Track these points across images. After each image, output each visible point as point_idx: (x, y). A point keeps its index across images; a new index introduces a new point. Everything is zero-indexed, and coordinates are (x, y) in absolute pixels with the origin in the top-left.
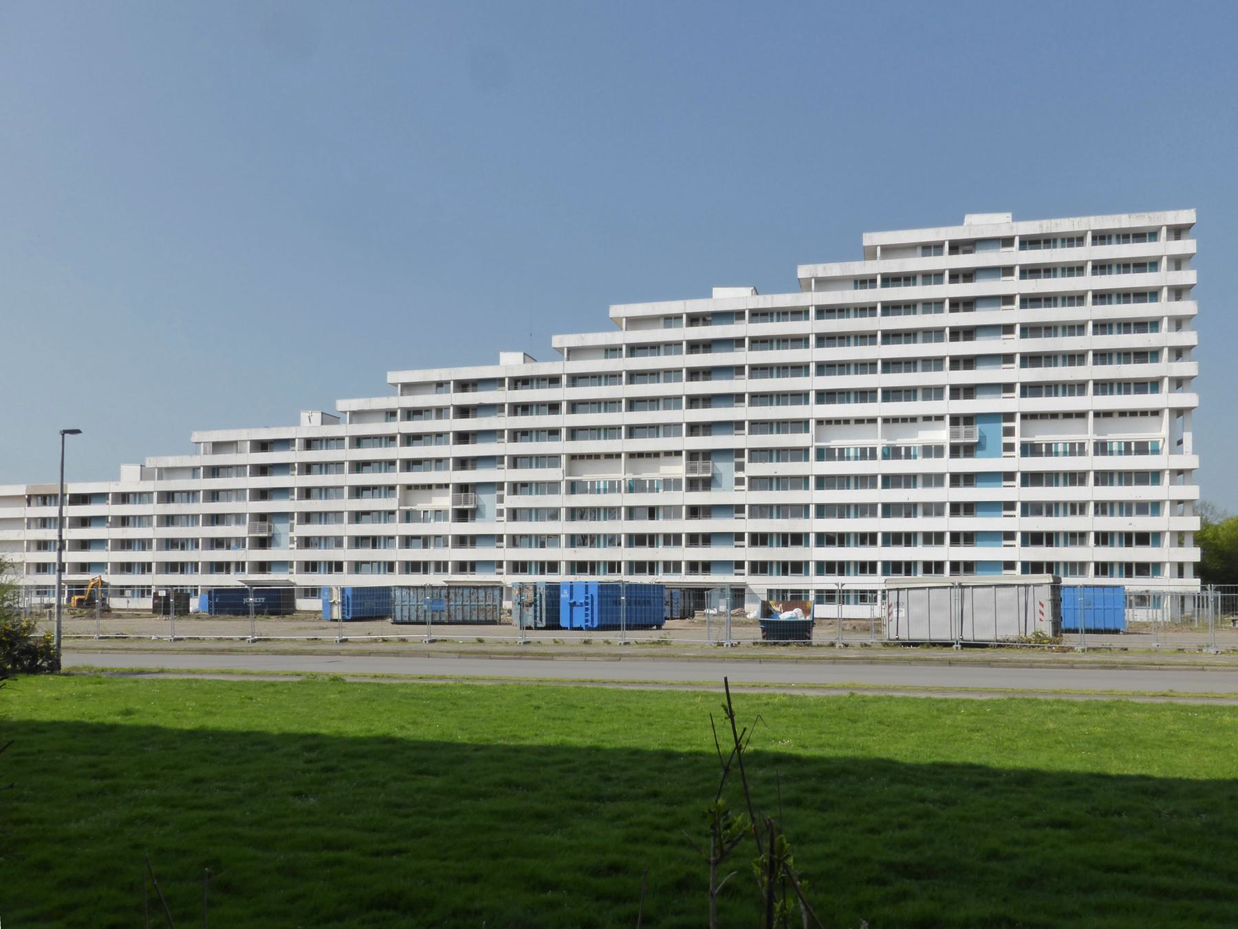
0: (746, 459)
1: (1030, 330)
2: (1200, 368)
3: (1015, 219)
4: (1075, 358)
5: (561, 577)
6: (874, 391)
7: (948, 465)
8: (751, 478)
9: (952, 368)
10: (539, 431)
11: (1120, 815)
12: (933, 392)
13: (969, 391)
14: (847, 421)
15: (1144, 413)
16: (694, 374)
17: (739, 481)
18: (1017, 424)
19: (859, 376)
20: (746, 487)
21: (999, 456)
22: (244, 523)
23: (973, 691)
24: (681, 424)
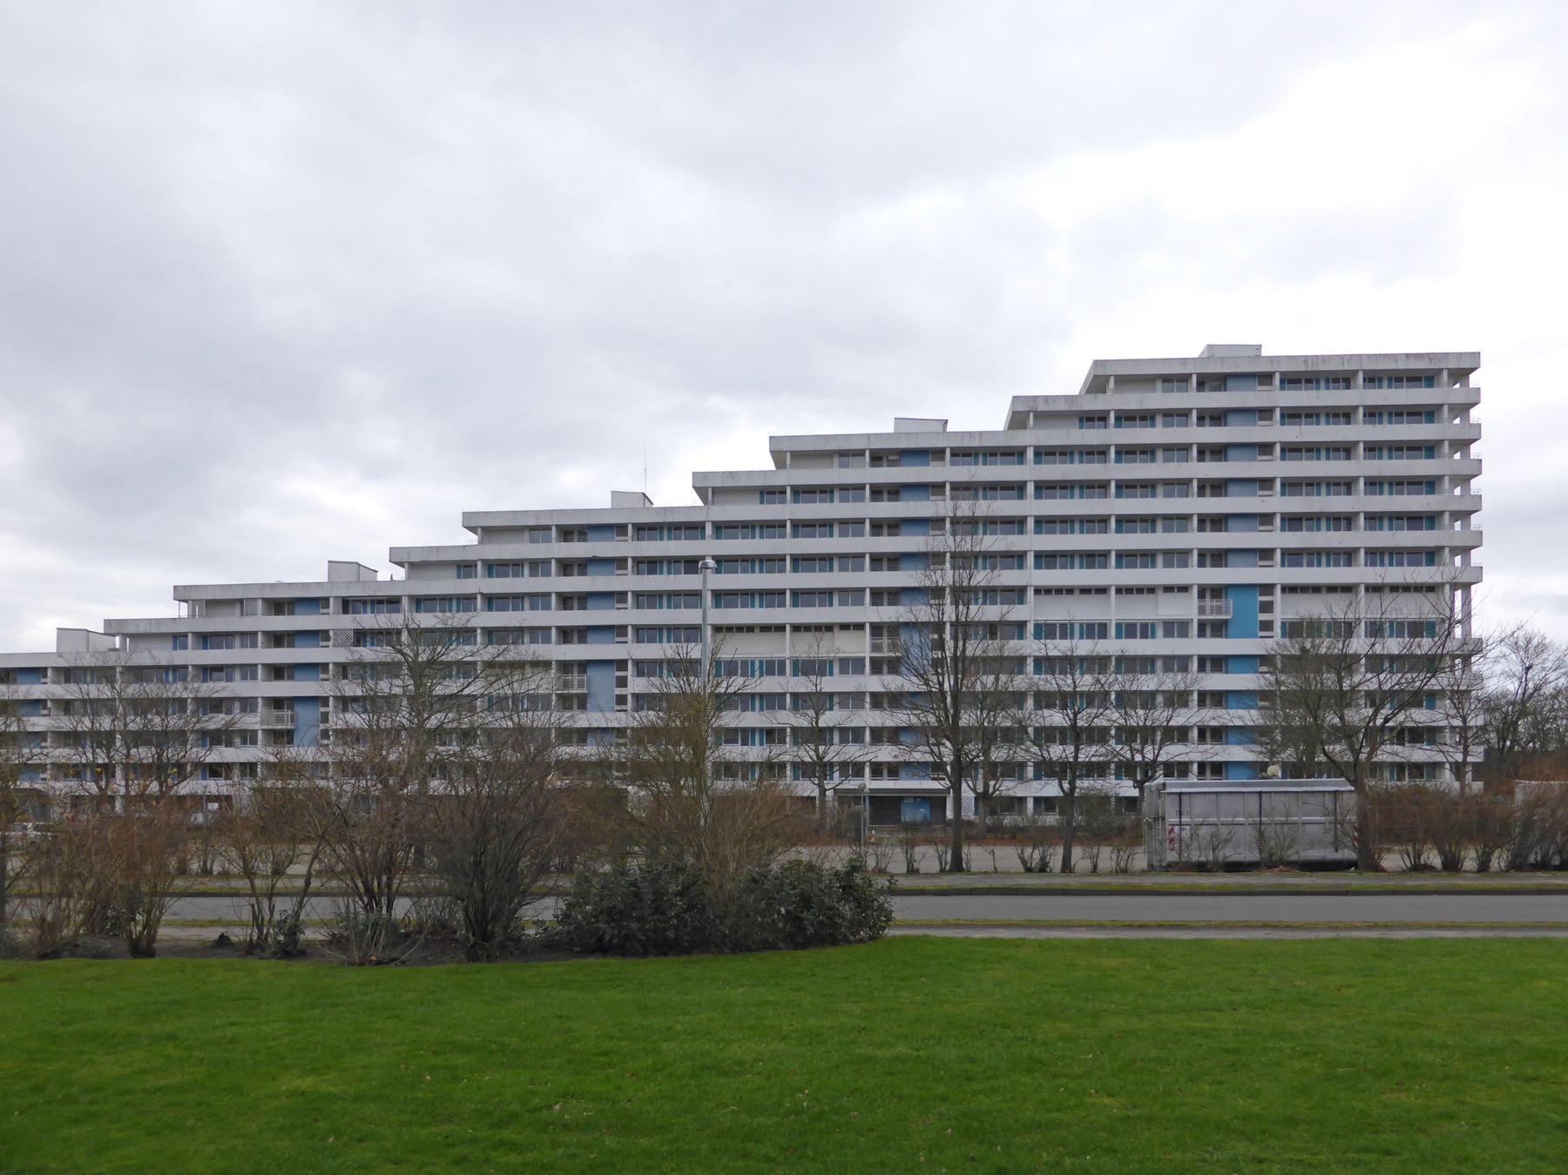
0: (331, 708)
1: (1293, 486)
4: (1343, 521)
8: (636, 697)
9: (873, 569)
10: (672, 594)
11: (550, 1107)
12: (1177, 557)
13: (1218, 557)
16: (878, 526)
18: (630, 672)
19: (1085, 536)
21: (1255, 636)
23: (975, 925)
24: (863, 590)
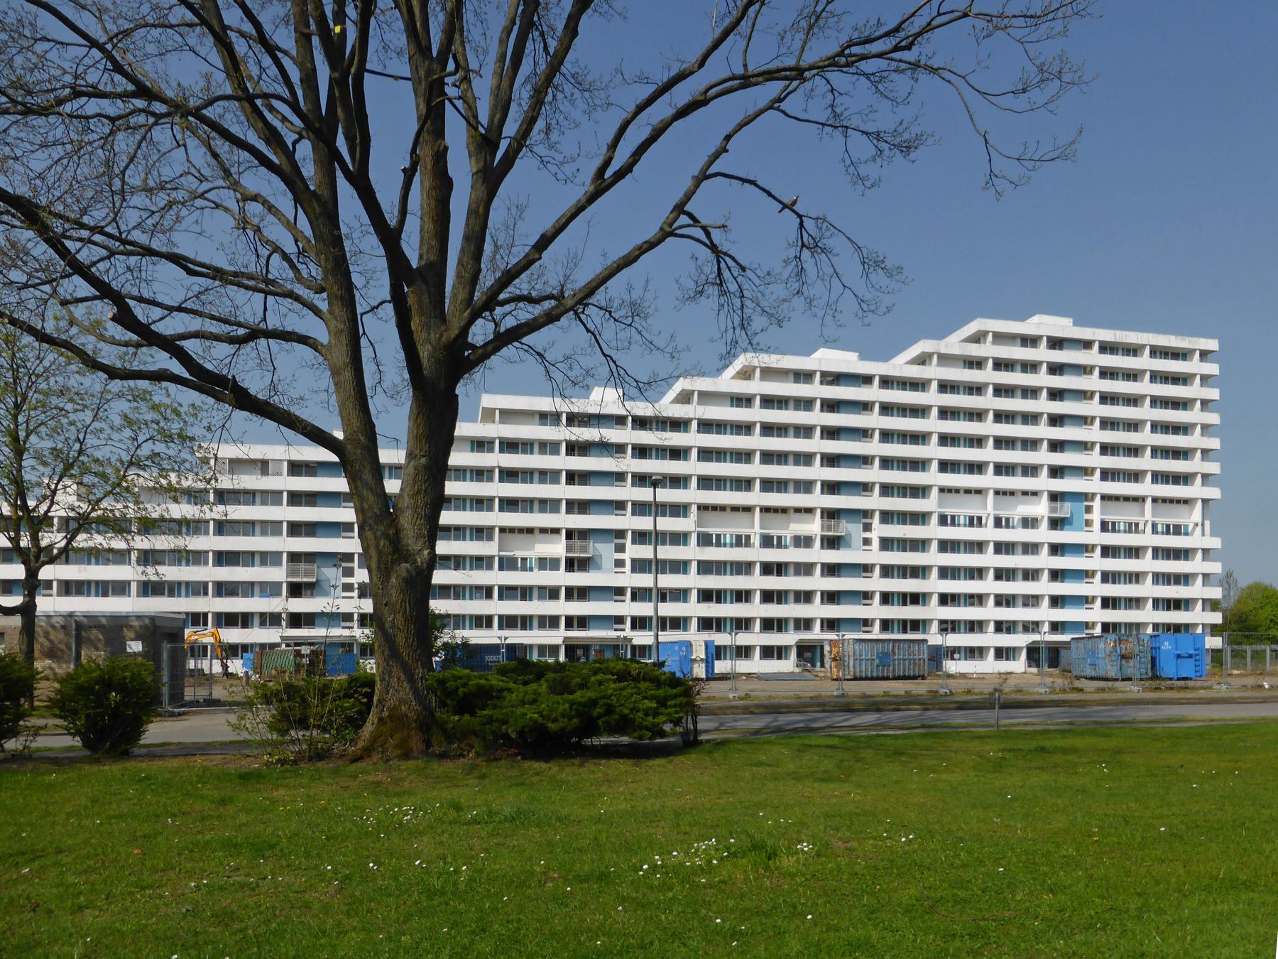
2: (1222, 468)
3: (1075, 324)
5: (816, 633)
6: (491, 499)
7: (563, 578)
8: (633, 560)
14: (957, 491)
15: (1178, 501)
17: (347, 588)
18: (1097, 504)
20: (355, 594)
22: (281, 564)
